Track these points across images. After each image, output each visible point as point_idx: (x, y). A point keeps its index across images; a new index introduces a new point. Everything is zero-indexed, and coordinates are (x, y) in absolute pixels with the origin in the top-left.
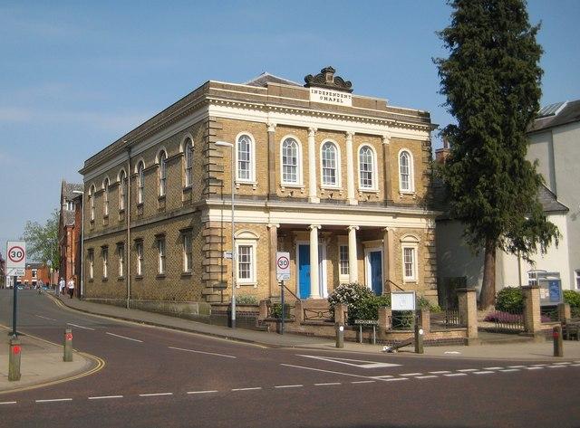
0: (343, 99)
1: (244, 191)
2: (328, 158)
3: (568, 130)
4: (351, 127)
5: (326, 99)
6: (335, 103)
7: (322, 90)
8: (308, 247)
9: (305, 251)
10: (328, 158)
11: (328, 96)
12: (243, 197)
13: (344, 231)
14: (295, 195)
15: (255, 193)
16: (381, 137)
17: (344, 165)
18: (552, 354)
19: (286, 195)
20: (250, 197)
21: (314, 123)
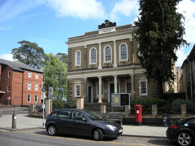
0: (112, 30)
1: (77, 69)
2: (108, 52)
3: (5, 60)
4: (114, 39)
5: (104, 31)
6: (108, 32)
7: (103, 29)
8: (113, 84)
9: (112, 86)
10: (108, 52)
11: (105, 30)
12: (77, 70)
13: (111, 78)
14: (94, 67)
15: (80, 69)
16: (128, 39)
17: (113, 53)
18: (11, 127)
19: (121, 65)
20: (79, 70)
21: (99, 41)
